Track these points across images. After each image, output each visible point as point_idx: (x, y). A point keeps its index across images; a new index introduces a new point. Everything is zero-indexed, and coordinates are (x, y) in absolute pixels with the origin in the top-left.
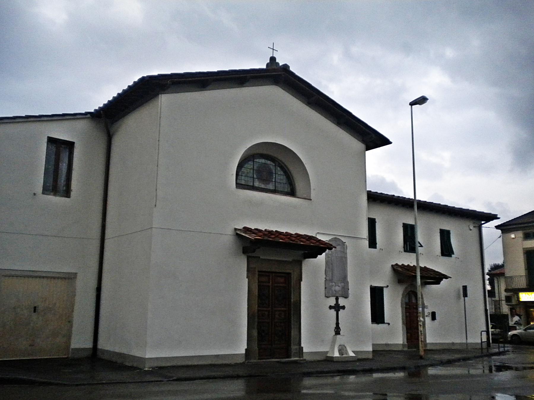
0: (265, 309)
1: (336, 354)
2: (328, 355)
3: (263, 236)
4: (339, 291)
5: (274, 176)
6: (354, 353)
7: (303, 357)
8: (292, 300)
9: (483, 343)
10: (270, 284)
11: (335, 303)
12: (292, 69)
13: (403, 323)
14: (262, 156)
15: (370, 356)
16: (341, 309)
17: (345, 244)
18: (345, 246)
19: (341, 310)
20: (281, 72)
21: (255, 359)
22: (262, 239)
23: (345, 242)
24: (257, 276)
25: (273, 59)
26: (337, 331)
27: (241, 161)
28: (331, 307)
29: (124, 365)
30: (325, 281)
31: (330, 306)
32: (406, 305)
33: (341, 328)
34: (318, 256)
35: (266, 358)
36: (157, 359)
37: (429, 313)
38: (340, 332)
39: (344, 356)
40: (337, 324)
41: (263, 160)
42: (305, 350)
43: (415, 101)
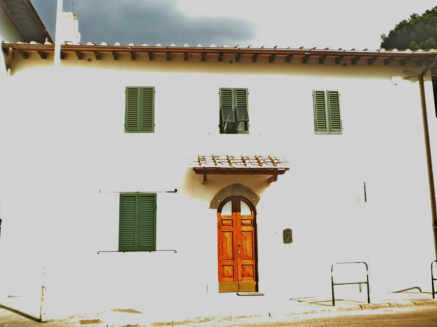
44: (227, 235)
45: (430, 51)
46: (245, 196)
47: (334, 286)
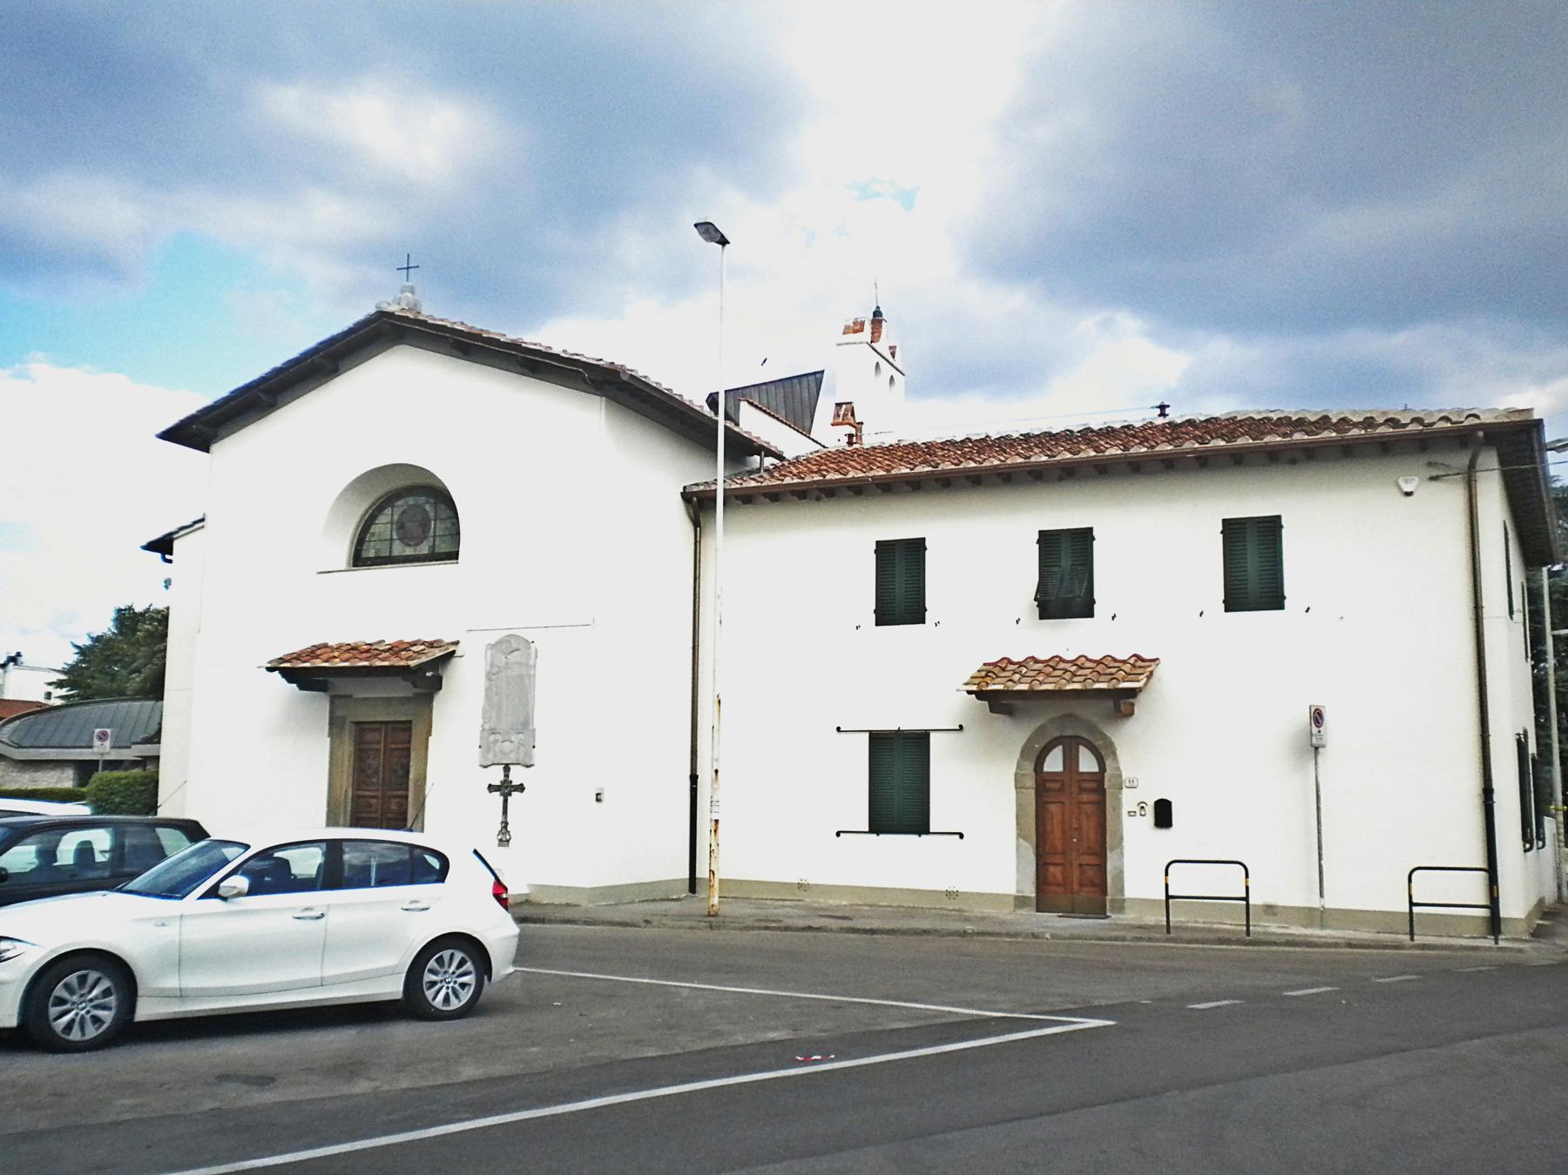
9: (1171, 901)
28: (491, 788)
31: (490, 786)
37: (1141, 815)
44: (1053, 808)
45: (1265, 440)
46: (1085, 736)
47: (1244, 895)
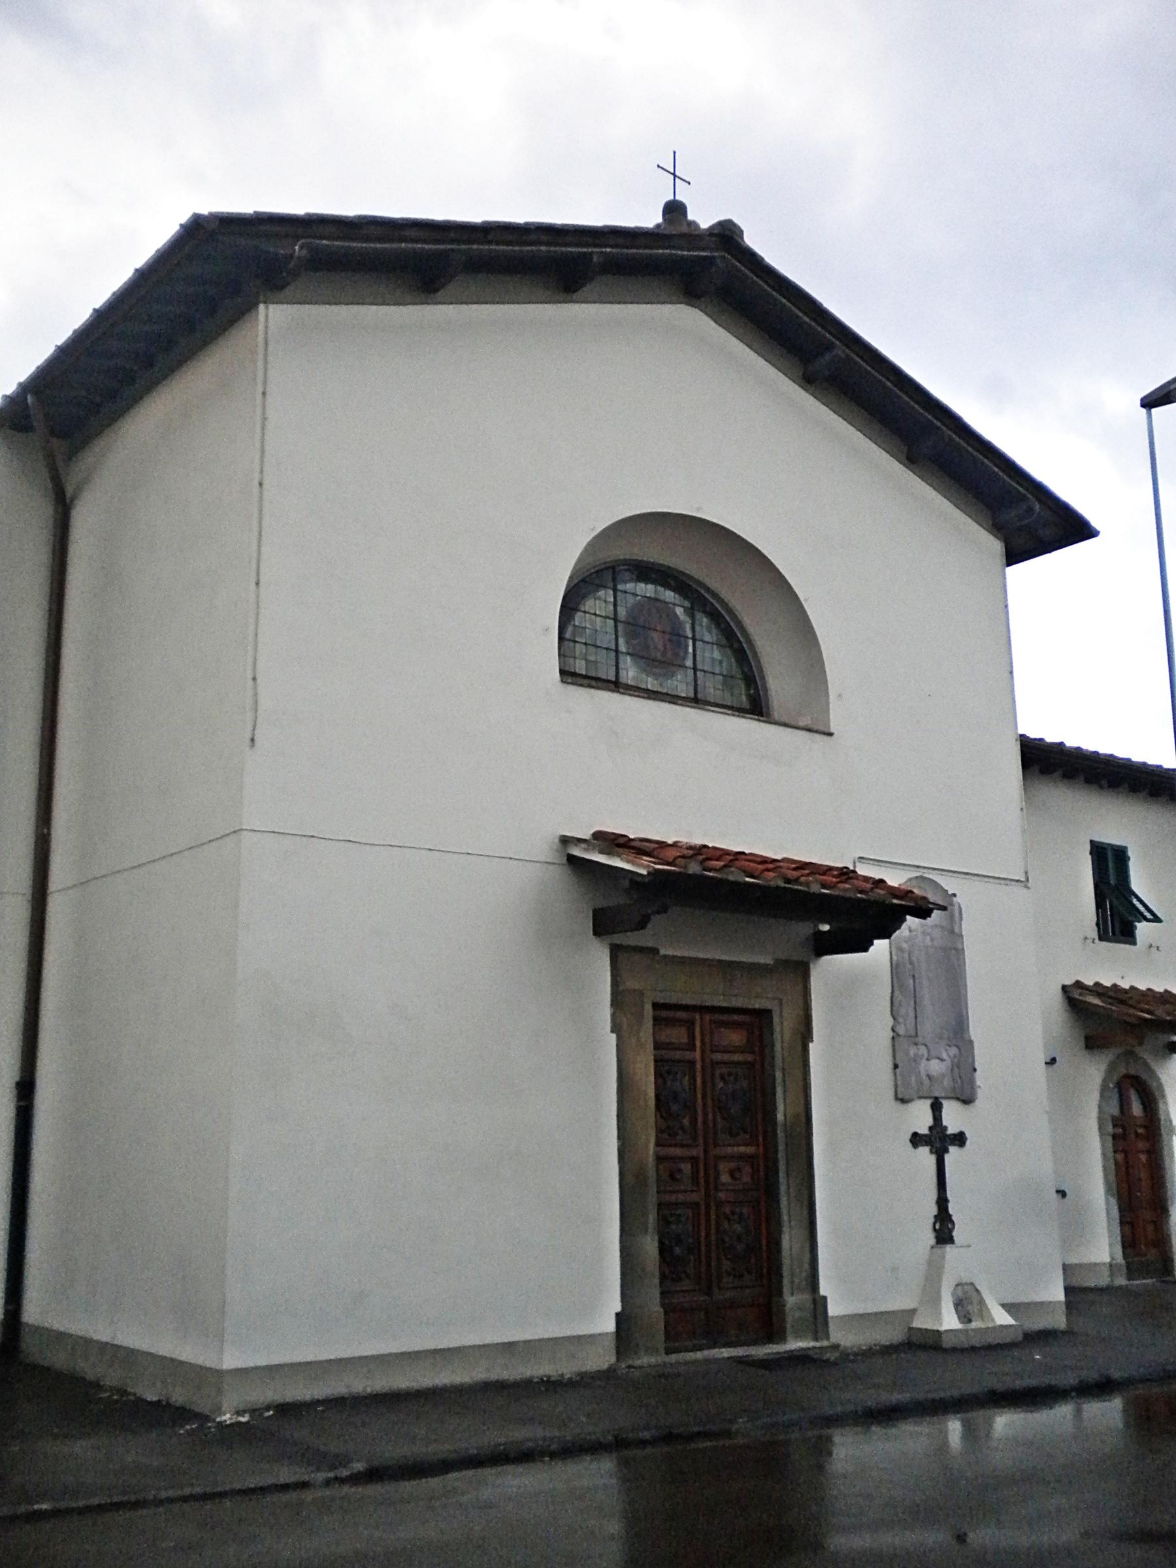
0: (678, 1151)
1: (949, 1321)
2: (917, 1324)
3: (680, 861)
4: (943, 1076)
5: (690, 650)
6: (1008, 1311)
7: (828, 1337)
8: (780, 1117)
10: (698, 1055)
11: (929, 1121)
12: (751, 240)
13: (1108, 1191)
14: (645, 571)
15: (1059, 1321)
16: (953, 1144)
17: (955, 899)
18: (957, 906)
19: (952, 1149)
20: (712, 250)
21: (653, 1351)
22: (680, 873)
23: (954, 895)
24: (648, 1024)
25: (674, 210)
26: (944, 1230)
27: (577, 568)
28: (916, 1140)
29: (132, 1398)
30: (893, 1038)
31: (915, 1135)
32: (1114, 1126)
33: (954, 1218)
34: (876, 942)
35: (689, 1344)
36: (272, 1370)
38: (954, 1234)
39: (973, 1325)
40: (942, 1202)
41: (650, 587)
42: (834, 1309)
43: (1165, 391)
